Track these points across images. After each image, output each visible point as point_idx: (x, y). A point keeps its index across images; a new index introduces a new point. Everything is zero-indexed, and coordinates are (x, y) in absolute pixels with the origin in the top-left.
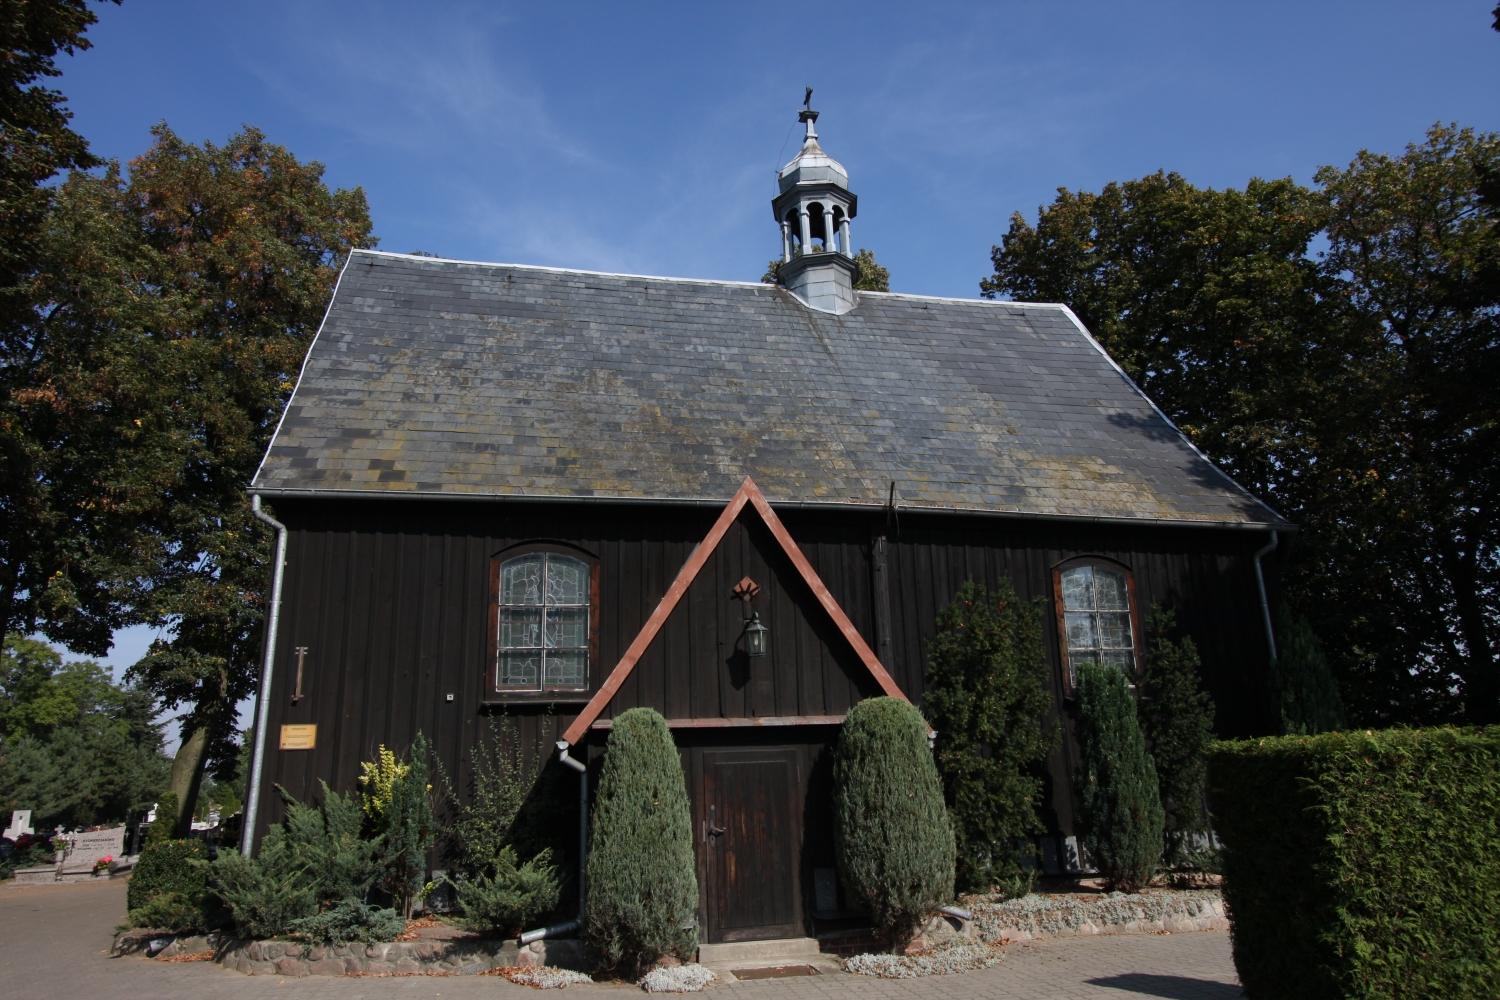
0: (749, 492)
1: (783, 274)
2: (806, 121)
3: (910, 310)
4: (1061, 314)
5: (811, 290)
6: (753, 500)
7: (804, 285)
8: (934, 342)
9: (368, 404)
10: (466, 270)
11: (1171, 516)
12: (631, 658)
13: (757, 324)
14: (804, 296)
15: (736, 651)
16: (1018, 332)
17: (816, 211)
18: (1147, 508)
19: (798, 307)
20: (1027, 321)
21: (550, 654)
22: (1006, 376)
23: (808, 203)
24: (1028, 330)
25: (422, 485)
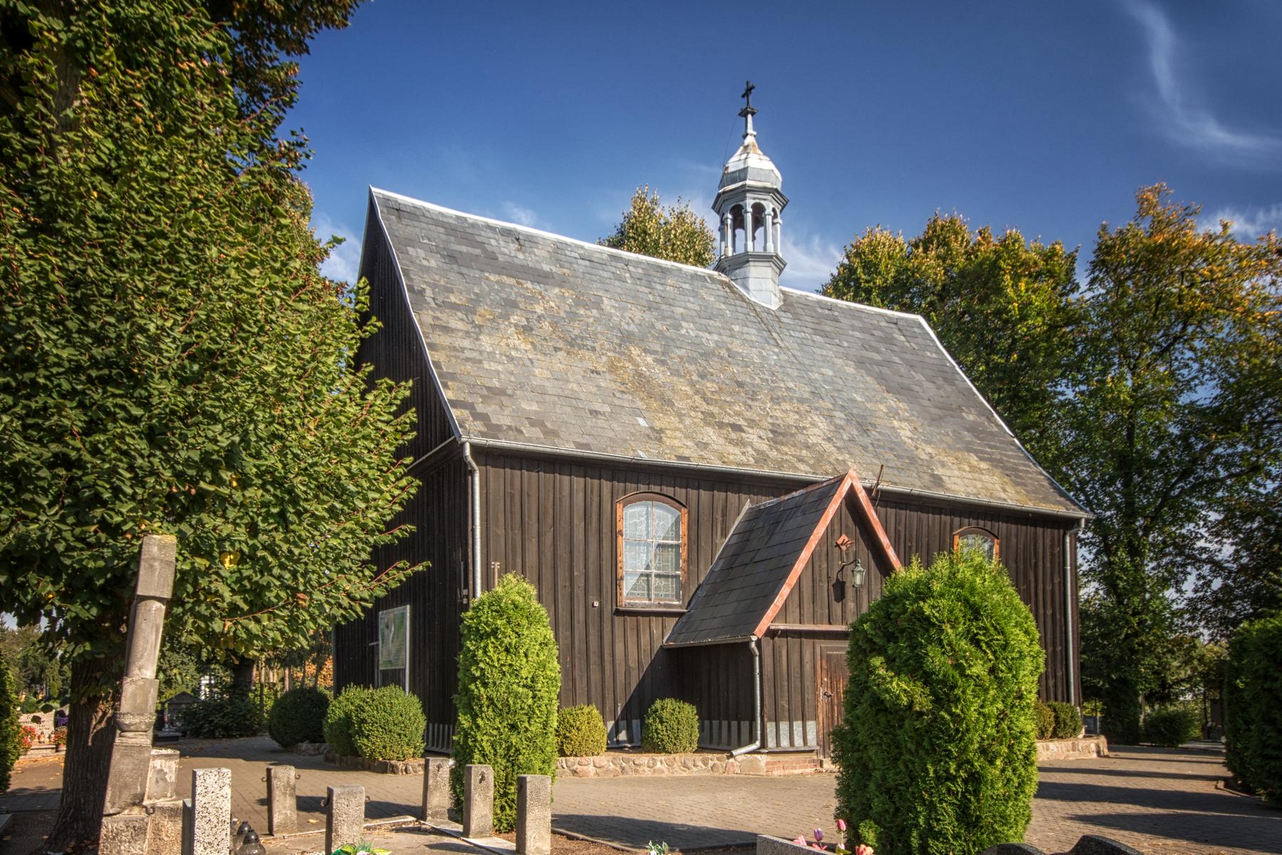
0: (852, 478)
1: (726, 264)
2: (746, 116)
3: (820, 310)
4: (920, 326)
5: (752, 283)
6: (855, 483)
7: (746, 278)
8: (845, 344)
9: (486, 365)
10: (474, 225)
11: (1030, 506)
12: (790, 585)
13: (721, 313)
14: (746, 288)
15: (837, 579)
16: (895, 339)
17: (759, 209)
18: (1009, 496)
19: (742, 298)
20: (899, 330)
21: (658, 576)
22: (464, 270)
23: (753, 202)
24: (902, 338)
25: (579, 445)
